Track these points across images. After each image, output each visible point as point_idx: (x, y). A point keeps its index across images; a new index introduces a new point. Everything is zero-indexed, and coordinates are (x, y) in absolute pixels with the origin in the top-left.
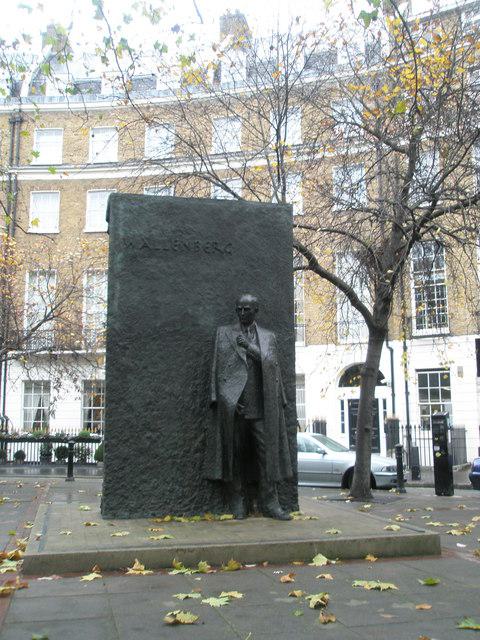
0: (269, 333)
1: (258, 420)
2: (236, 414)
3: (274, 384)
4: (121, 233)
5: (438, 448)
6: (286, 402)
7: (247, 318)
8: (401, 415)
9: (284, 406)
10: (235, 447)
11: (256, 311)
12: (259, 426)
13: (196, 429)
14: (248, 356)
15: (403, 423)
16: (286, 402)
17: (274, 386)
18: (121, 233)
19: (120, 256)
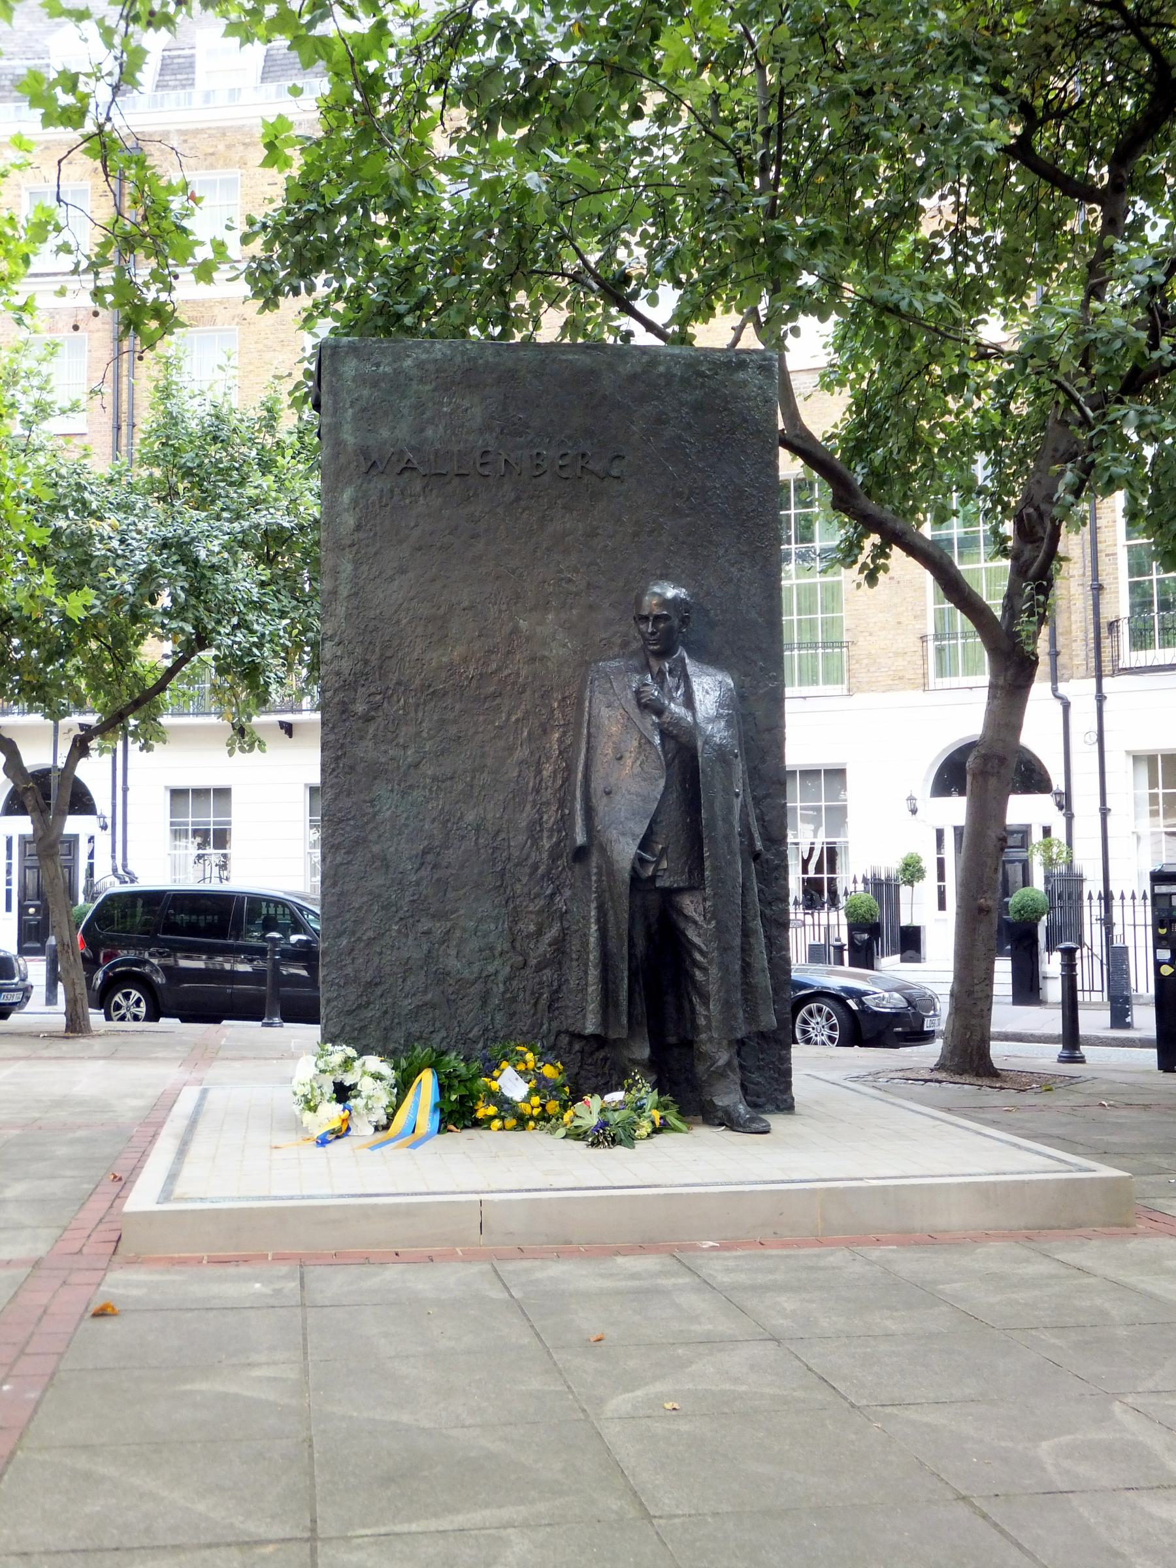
0: (719, 677)
1: (691, 889)
2: (635, 878)
3: (728, 800)
4: (349, 437)
5: (1165, 954)
6: (759, 845)
7: (668, 641)
8: (1087, 863)
9: (756, 856)
10: (631, 956)
11: (684, 621)
12: (690, 905)
13: (540, 912)
14: (664, 735)
15: (1093, 886)
16: (759, 845)
17: (729, 809)
18: (349, 437)
19: (347, 496)
